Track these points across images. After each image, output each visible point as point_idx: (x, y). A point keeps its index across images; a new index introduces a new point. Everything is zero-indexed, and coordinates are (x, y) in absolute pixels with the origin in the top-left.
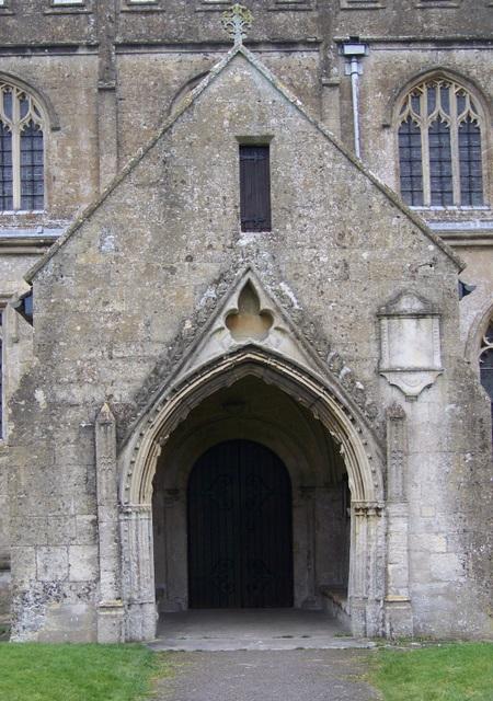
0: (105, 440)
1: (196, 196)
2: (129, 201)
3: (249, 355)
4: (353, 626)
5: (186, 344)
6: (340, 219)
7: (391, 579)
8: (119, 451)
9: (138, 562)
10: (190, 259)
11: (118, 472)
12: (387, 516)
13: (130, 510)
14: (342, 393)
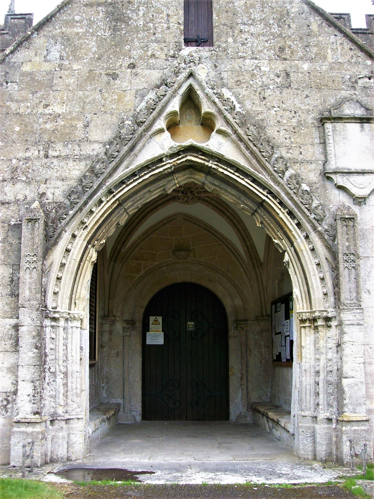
0: (33, 237)
1: (141, 13)
2: (77, 18)
3: (189, 158)
4: (301, 447)
5: (127, 140)
6: (280, 35)
7: (347, 395)
8: (47, 251)
9: (66, 374)
10: (133, 66)
11: (44, 272)
12: (340, 324)
13: (57, 315)
14: (288, 194)
